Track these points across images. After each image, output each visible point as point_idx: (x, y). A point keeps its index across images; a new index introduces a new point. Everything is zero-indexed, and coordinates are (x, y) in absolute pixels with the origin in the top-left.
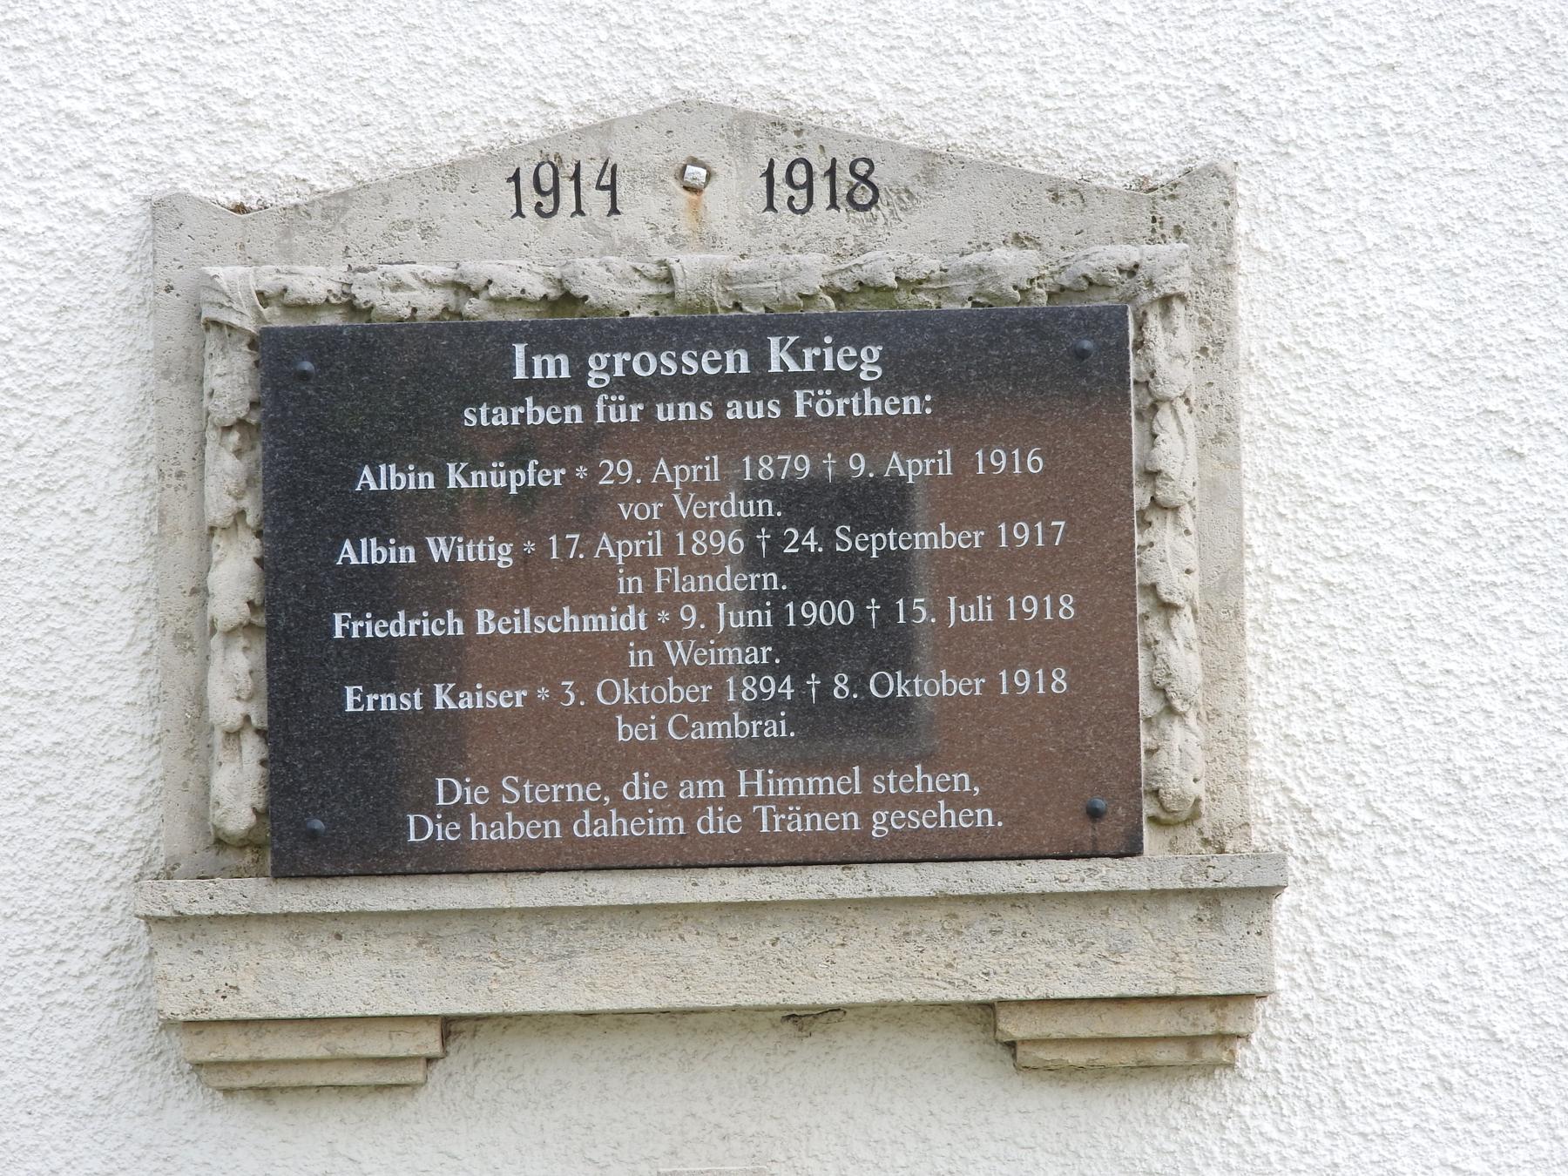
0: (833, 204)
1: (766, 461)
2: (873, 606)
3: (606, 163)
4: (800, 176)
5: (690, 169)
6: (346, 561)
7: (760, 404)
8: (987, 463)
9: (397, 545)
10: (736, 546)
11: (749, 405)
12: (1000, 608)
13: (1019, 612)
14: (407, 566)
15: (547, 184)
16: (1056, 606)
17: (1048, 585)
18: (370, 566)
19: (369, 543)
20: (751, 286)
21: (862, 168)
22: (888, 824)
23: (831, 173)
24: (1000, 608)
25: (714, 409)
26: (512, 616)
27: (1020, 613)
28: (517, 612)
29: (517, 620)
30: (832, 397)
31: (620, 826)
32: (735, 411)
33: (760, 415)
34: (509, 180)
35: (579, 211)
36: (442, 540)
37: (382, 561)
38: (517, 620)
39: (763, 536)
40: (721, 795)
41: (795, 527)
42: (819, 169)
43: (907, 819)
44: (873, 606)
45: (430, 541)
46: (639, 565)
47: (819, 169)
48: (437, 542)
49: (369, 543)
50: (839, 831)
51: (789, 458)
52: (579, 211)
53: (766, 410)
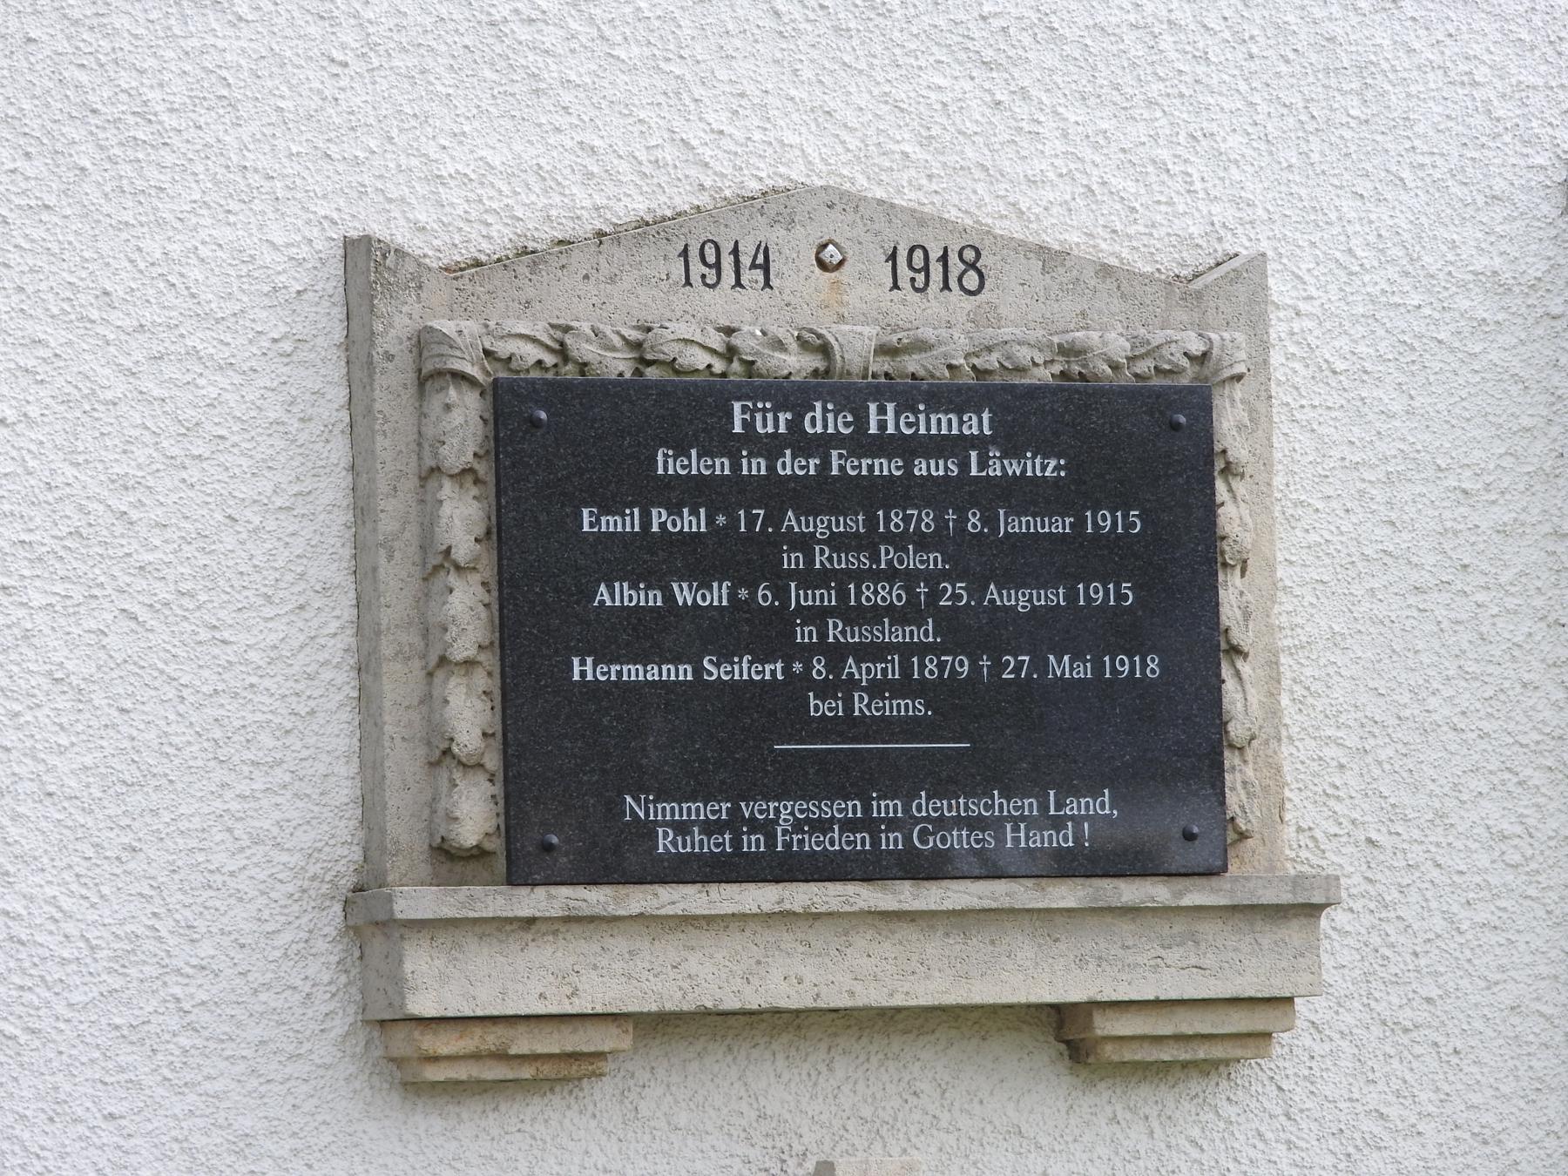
0: (946, 287)
1: (897, 515)
2: (985, 662)
3: (759, 246)
4: (918, 260)
5: (831, 247)
6: (602, 602)
7: (941, 462)
8: (1095, 523)
9: (647, 589)
10: (899, 597)
11: (932, 462)
12: (1099, 667)
13: (1114, 670)
14: (654, 609)
15: (711, 259)
16: (1144, 665)
17: (1135, 645)
18: (623, 608)
19: (622, 586)
20: (1077, 334)
21: (969, 255)
22: (792, 814)
23: (944, 259)
24: (1099, 667)
25: (958, 466)
26: (732, 663)
27: (1114, 670)
28: (736, 659)
29: (736, 667)
30: (1000, 458)
31: (701, 841)
32: (921, 468)
33: (941, 473)
34: (680, 256)
35: (738, 283)
36: (685, 585)
37: (633, 604)
38: (736, 667)
39: (922, 589)
40: (867, 848)
41: (947, 581)
42: (935, 254)
43: (808, 809)
44: (985, 662)
45: (675, 586)
46: (818, 616)
47: (935, 254)
48: (680, 586)
49: (622, 586)
50: (766, 819)
51: (916, 512)
52: (738, 283)
53: (946, 468)
